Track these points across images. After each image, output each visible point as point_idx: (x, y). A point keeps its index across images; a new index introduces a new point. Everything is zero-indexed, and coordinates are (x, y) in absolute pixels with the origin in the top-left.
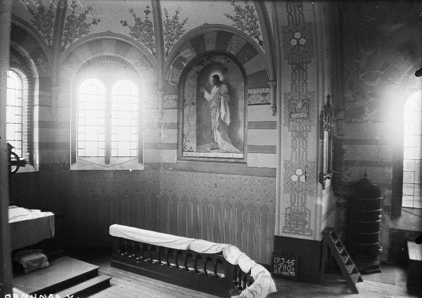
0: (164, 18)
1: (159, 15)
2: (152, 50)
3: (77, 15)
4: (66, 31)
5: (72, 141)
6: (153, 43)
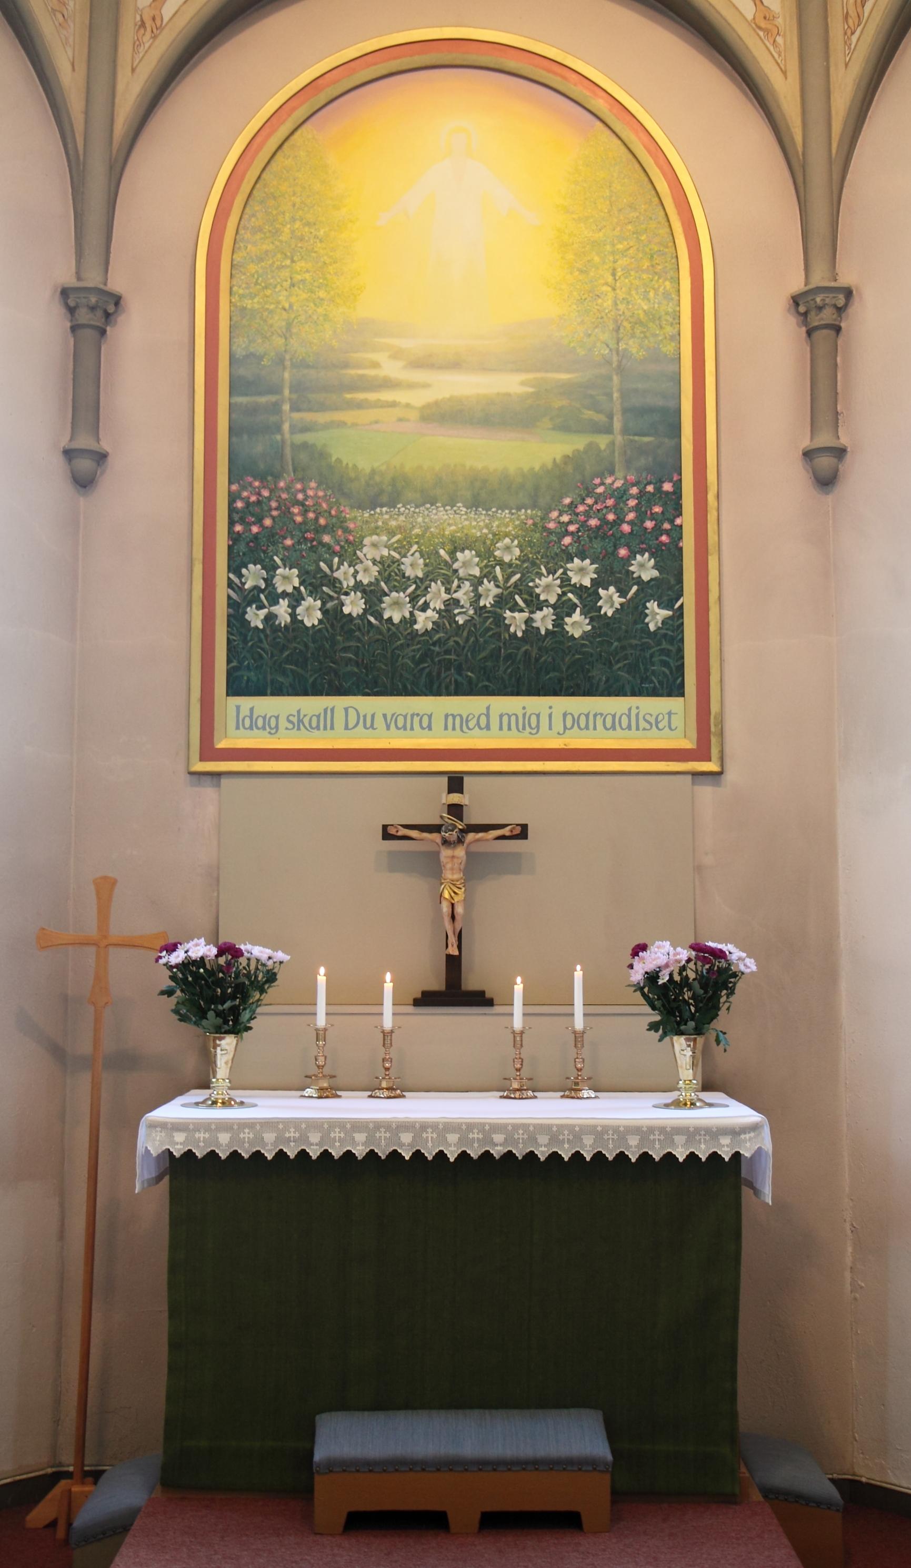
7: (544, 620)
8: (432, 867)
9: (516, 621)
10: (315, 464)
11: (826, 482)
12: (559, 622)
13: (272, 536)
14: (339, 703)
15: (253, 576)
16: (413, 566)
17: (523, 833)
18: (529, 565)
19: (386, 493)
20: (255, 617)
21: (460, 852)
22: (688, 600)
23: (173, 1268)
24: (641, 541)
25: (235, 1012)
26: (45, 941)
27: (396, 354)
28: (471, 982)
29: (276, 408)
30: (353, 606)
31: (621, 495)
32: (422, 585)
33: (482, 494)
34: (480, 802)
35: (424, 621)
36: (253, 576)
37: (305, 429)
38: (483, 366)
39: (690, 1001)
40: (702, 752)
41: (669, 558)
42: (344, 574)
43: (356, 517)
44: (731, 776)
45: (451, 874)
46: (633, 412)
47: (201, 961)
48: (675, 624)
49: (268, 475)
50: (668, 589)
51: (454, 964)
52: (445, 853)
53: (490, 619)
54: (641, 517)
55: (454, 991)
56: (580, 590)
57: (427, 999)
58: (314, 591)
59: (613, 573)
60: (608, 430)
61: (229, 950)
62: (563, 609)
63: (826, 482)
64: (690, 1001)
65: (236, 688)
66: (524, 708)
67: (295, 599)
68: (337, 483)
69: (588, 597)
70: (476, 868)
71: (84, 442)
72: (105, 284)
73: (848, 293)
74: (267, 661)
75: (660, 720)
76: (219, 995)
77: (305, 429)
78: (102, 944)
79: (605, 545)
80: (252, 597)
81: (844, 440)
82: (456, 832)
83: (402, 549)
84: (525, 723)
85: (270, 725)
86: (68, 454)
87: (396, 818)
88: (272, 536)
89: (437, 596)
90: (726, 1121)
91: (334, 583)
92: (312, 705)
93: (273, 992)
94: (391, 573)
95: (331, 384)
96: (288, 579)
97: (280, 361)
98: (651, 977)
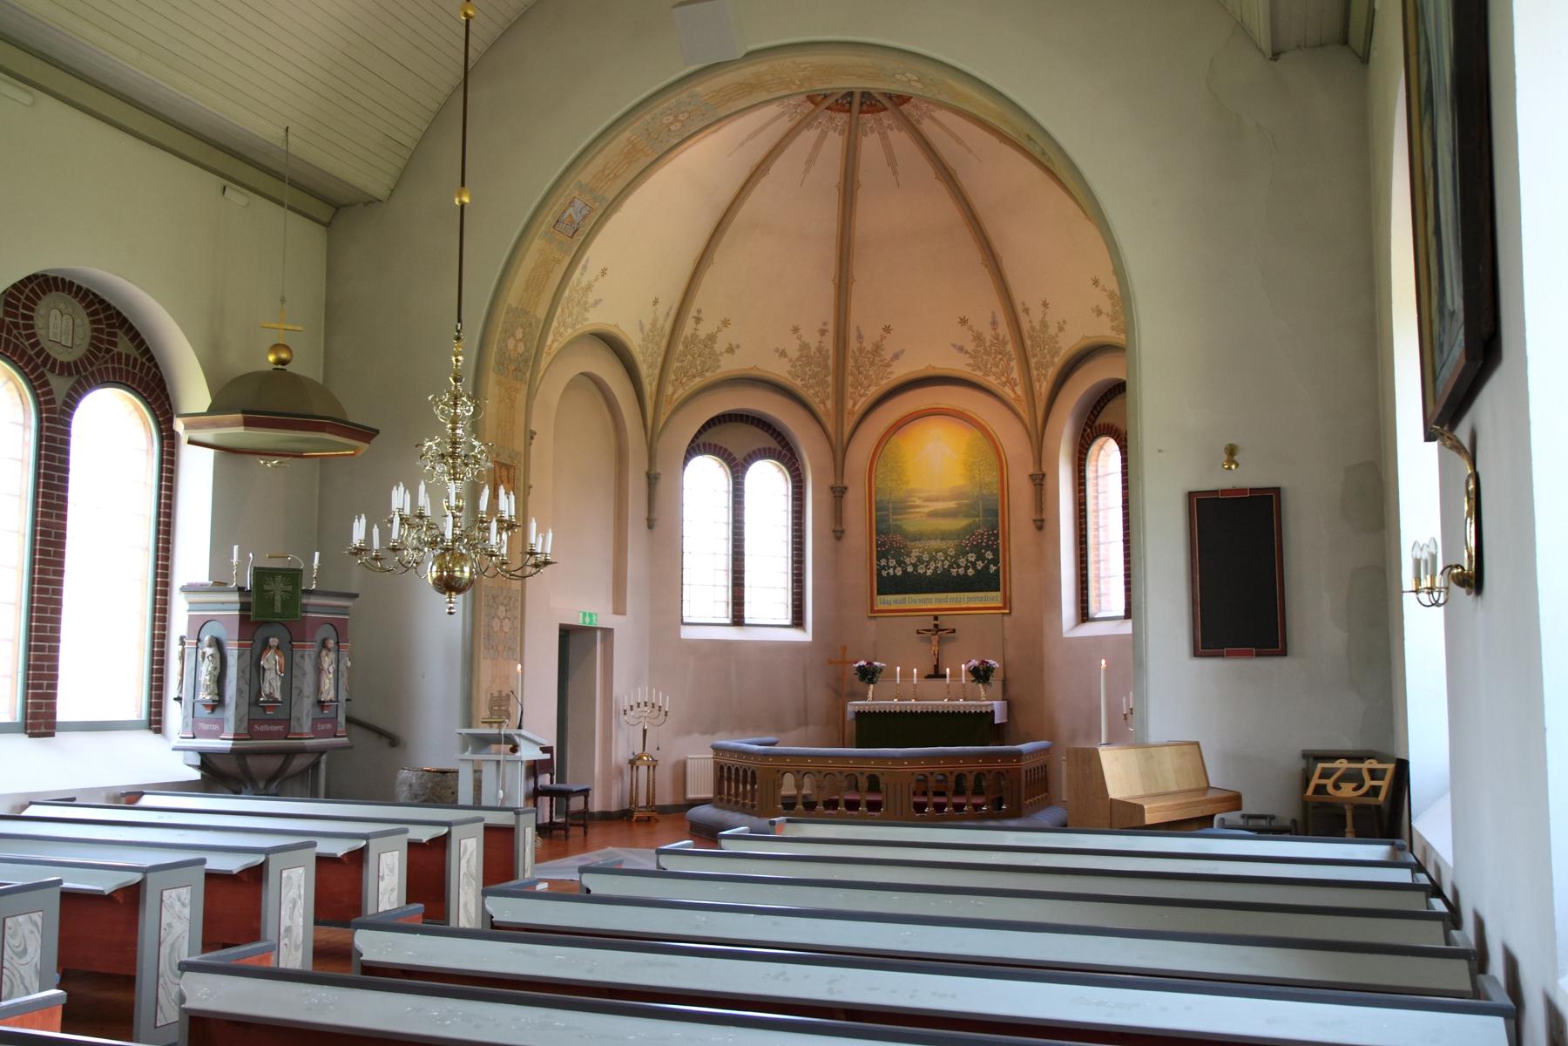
0: (853, 344)
3: (1037, 325)
7: (961, 571)
8: (930, 641)
9: (954, 572)
10: (899, 530)
13: (888, 551)
15: (883, 562)
16: (926, 557)
18: (957, 556)
19: (918, 537)
20: (884, 573)
24: (988, 548)
26: (830, 662)
30: (910, 569)
33: (944, 536)
34: (945, 623)
35: (929, 573)
36: (883, 562)
38: (944, 499)
41: (996, 552)
42: (907, 560)
46: (986, 510)
48: (997, 571)
50: (995, 561)
53: (947, 572)
55: (937, 674)
57: (929, 677)
59: (980, 557)
61: (869, 663)
62: (967, 568)
65: (880, 593)
68: (905, 535)
69: (974, 564)
72: (738, 620)
74: (887, 585)
75: (993, 598)
76: (868, 674)
79: (978, 549)
80: (884, 568)
84: (957, 600)
85: (888, 603)
88: (888, 551)
89: (932, 566)
94: (920, 559)
95: (902, 507)
96: (892, 562)
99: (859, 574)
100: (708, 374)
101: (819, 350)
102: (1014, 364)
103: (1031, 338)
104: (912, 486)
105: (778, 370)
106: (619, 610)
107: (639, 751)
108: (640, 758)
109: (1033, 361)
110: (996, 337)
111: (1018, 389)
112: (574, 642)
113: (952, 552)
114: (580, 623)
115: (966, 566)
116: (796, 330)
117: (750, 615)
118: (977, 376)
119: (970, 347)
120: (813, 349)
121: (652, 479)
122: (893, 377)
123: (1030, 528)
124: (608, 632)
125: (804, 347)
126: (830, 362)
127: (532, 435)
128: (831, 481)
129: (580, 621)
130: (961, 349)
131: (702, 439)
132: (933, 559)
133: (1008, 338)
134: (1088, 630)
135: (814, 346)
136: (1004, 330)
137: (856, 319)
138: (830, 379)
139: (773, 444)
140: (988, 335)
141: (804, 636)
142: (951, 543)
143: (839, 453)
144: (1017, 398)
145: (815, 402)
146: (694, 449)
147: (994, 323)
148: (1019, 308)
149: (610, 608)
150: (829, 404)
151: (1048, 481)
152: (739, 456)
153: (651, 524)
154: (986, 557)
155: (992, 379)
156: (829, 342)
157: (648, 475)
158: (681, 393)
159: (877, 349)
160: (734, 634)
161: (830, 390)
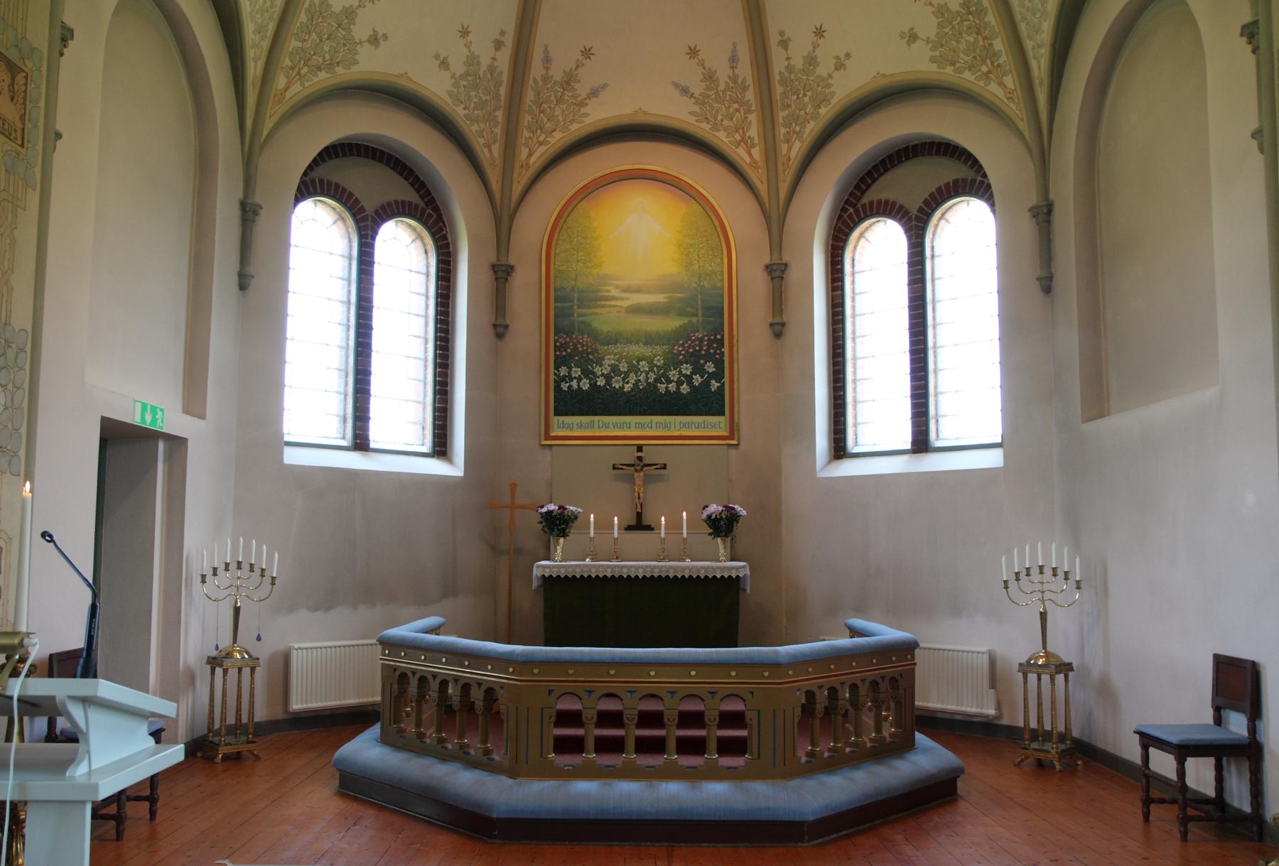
0: (536, 70)
1: (379, 91)
2: (1002, 84)
3: (798, 63)
4: (786, 112)
5: (335, 640)
6: (1001, 61)
7: (672, 387)
8: (631, 480)
11: (778, 335)
12: (678, 388)
13: (571, 356)
14: (596, 418)
15: (563, 371)
16: (623, 367)
17: (664, 467)
18: (666, 367)
19: (613, 339)
20: (564, 386)
21: (642, 474)
22: (726, 380)
23: (545, 615)
24: (708, 357)
25: (564, 530)
27: (617, 287)
28: (645, 522)
29: (571, 308)
31: (701, 340)
32: (627, 374)
33: (649, 339)
34: (649, 456)
35: (627, 388)
36: (563, 371)
37: (583, 315)
39: (723, 525)
40: (731, 437)
41: (719, 364)
42: (598, 370)
43: (602, 349)
44: (742, 446)
45: (639, 482)
47: (551, 512)
48: (721, 388)
49: (569, 333)
50: (719, 375)
51: (639, 515)
52: (636, 474)
53: (652, 387)
54: (709, 348)
55: (639, 524)
56: (685, 376)
57: (629, 528)
58: (586, 376)
59: (698, 369)
60: (696, 315)
62: (679, 383)
63: (778, 335)
64: (723, 525)
65: (556, 414)
66: (693, 52)
67: (579, 379)
68: (595, 335)
69: (689, 379)
70: (647, 480)
71: (500, 321)
72: (360, 443)
73: (786, 265)
74: (569, 403)
75: (715, 425)
76: (558, 524)
77: (583, 315)
78: (512, 507)
79: (695, 359)
80: (563, 379)
81: (785, 320)
82: (640, 466)
83: (619, 360)
84: (665, 426)
86: (495, 326)
87: (618, 461)
88: (571, 356)
89: (632, 378)
90: (738, 568)
91: (594, 373)
92: (586, 419)
93: (576, 523)
94: (615, 369)
95: (592, 298)
96: (576, 372)
97: (573, 290)
98: (709, 517)
99: (528, 387)
100: (339, 70)
101: (492, 69)
102: (753, 118)
103: (784, 82)
104: (607, 269)
105: (436, 86)
106: (194, 403)
107: (225, 642)
108: (229, 655)
109: (781, 115)
110: (734, 79)
111: (756, 153)
112: (123, 447)
113: (659, 361)
114: (137, 420)
115: (677, 381)
116: (465, 32)
117: (376, 437)
118: (702, 130)
119: (697, 89)
120: (484, 67)
121: (248, 213)
122: (588, 120)
123: (765, 334)
124: (177, 443)
125: (473, 60)
126: (503, 91)
127: (66, 36)
128: (492, 257)
129: (136, 418)
130: (685, 91)
131: (318, 173)
132: (633, 369)
133: (749, 81)
134: (847, 468)
135: (485, 63)
136: (745, 70)
137: (545, 33)
138: (500, 114)
139: (413, 197)
140: (723, 74)
141: (453, 469)
142: (659, 350)
143: (503, 219)
144: (754, 164)
145: (478, 144)
146: (306, 189)
147: (733, 60)
148: (774, 39)
149: (179, 406)
150: (496, 149)
151: (793, 276)
152: (370, 206)
153: (244, 282)
154: (700, 371)
155: (722, 135)
156: (504, 61)
157: (244, 205)
158: (298, 91)
159: (569, 80)
160: (355, 461)
161: (498, 131)
